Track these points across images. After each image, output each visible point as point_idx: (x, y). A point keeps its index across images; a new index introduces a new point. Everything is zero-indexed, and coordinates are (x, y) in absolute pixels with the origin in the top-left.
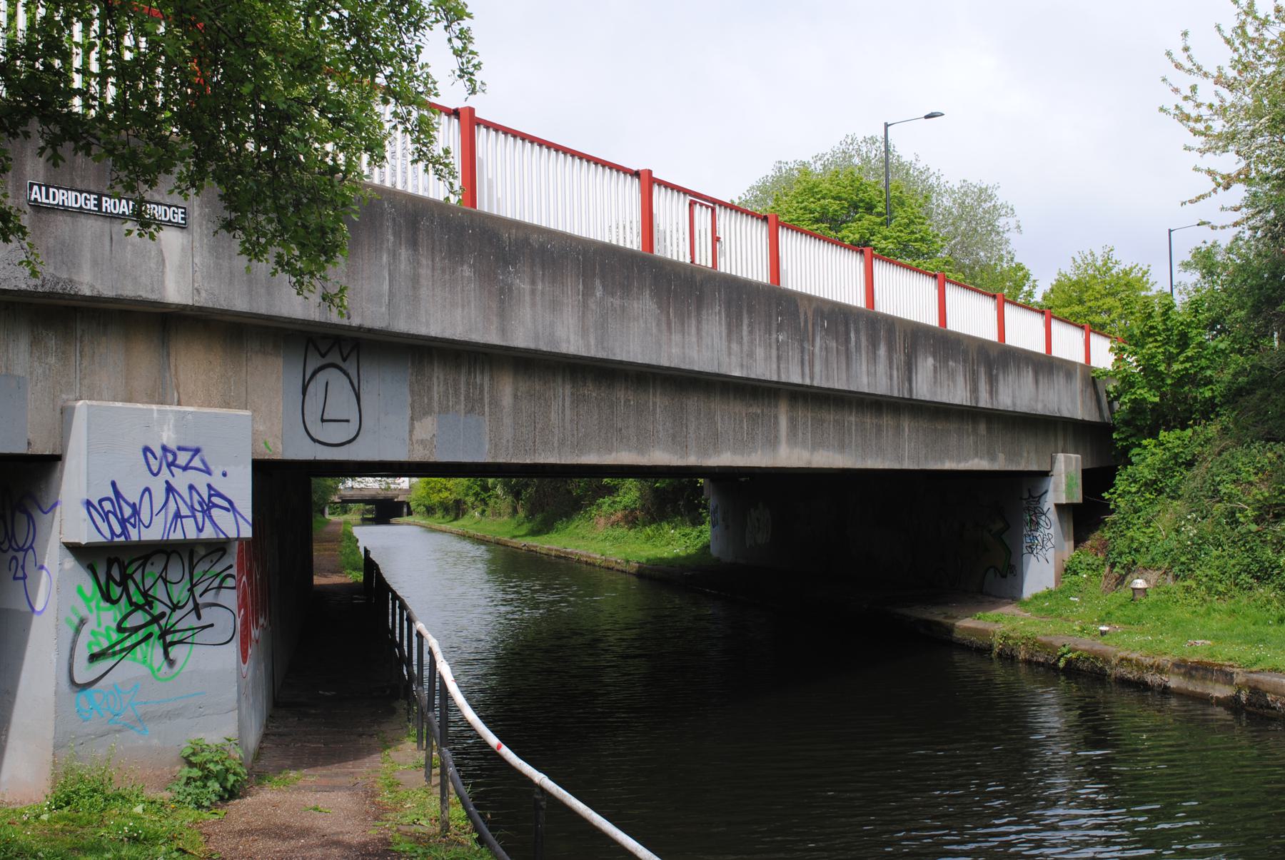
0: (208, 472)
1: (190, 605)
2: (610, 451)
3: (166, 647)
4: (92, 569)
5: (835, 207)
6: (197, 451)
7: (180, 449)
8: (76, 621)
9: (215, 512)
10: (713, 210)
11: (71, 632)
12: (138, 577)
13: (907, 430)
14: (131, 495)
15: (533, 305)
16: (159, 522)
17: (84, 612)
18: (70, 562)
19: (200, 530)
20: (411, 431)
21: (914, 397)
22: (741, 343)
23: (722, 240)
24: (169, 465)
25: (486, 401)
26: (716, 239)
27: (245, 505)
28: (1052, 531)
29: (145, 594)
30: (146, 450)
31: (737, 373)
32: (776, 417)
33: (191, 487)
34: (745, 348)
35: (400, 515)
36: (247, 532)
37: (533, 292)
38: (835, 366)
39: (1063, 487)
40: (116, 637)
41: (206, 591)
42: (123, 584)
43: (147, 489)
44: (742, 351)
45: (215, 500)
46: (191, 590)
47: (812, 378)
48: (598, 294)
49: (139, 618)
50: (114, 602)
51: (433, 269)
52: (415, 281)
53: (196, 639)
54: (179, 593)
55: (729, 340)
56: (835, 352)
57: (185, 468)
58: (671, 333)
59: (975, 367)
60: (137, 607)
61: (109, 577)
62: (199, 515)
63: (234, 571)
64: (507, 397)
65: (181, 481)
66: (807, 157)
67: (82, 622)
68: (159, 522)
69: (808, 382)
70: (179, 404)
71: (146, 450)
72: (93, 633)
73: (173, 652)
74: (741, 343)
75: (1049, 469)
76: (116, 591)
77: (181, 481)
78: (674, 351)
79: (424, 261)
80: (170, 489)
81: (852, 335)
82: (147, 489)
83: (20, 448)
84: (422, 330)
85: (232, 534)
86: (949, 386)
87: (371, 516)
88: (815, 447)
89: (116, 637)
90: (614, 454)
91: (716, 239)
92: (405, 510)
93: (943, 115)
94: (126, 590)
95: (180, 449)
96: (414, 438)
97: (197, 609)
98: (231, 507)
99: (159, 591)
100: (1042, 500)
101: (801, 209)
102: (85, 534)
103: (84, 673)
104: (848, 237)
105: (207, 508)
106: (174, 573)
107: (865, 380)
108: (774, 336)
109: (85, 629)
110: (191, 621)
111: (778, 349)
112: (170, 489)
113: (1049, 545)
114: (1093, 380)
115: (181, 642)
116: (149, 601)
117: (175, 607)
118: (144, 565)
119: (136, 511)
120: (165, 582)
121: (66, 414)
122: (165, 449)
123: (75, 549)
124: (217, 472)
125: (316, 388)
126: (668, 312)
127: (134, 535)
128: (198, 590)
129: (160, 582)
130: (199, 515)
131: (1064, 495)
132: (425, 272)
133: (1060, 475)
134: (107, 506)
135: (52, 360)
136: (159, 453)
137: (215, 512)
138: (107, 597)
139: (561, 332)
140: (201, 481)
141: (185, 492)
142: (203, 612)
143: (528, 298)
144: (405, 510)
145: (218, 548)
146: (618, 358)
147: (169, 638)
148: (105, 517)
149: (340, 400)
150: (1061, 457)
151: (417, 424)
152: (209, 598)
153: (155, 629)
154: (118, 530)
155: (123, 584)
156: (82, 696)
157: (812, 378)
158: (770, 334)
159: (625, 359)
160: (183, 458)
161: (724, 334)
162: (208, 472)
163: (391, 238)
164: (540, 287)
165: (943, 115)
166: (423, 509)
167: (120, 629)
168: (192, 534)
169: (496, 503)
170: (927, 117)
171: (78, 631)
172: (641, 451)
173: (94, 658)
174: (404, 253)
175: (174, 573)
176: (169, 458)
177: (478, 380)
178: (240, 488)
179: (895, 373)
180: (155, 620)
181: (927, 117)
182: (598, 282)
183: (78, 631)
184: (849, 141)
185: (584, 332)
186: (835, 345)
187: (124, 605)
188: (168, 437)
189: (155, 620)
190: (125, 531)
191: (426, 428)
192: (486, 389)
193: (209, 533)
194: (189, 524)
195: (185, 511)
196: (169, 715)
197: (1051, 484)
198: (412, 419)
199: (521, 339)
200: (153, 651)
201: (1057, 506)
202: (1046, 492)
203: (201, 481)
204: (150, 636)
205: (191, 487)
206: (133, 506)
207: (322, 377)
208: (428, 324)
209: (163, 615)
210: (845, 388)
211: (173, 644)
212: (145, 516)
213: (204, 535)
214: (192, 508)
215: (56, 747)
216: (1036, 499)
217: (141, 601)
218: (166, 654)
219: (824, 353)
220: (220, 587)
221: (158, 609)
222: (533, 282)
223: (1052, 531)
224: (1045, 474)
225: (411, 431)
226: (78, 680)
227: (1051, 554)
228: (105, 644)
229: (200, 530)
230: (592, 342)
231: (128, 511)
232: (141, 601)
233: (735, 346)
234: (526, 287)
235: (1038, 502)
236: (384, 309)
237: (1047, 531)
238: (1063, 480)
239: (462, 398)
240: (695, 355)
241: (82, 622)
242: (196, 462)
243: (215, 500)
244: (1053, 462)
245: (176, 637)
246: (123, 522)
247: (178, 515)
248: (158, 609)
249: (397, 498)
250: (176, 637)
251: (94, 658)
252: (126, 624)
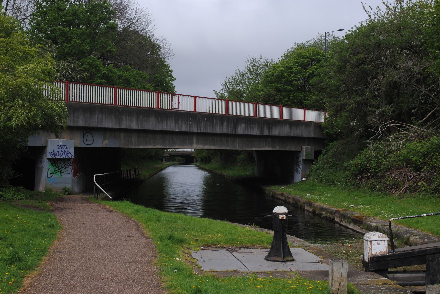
0: (67, 149)
1: (65, 167)
2: (146, 146)
3: (61, 173)
4: (50, 162)
5: (306, 61)
6: (65, 146)
7: (63, 145)
8: (48, 168)
9: (68, 154)
10: (178, 96)
11: (48, 170)
12: (57, 163)
13: (238, 141)
14: (56, 152)
15: (126, 121)
16: (60, 155)
17: (49, 167)
18: (47, 161)
19: (66, 157)
20: (103, 142)
21: (237, 133)
22: (179, 124)
23: (180, 102)
24: (61, 148)
25: (118, 137)
26: (179, 102)
27: (73, 154)
28: (301, 166)
29: (58, 166)
30: (58, 146)
31: (177, 130)
32: (192, 139)
33: (64, 151)
34: (180, 125)
35: (193, 162)
36: (73, 157)
37: (126, 119)
38: (208, 128)
39: (304, 155)
40: (54, 171)
41: (67, 166)
42: (55, 164)
43: (58, 151)
44: (179, 126)
45: (68, 153)
46: (65, 165)
47: (200, 130)
48: (141, 118)
49: (57, 169)
50: (54, 166)
51: (106, 117)
52: (102, 119)
53: (65, 172)
54: (63, 166)
55: (175, 124)
56: (208, 125)
57: (64, 148)
58: (159, 124)
59: (262, 126)
60: (57, 167)
61: (53, 163)
62: (66, 155)
63: (72, 163)
64: (122, 137)
65: (63, 150)
66: (304, 42)
67: (49, 169)
68: (60, 155)
69: (199, 131)
70: (63, 139)
71: (58, 146)
72: (51, 170)
73: (62, 174)
74: (179, 124)
75: (301, 150)
76: (54, 165)
77: (63, 150)
78: (160, 127)
79: (104, 115)
80: (61, 151)
81: (215, 121)
82: (58, 151)
83: (41, 145)
84: (103, 127)
85: (71, 158)
86: (251, 130)
87: (183, 162)
88: (204, 145)
89: (54, 171)
90: (147, 146)
91: (179, 102)
92: (195, 160)
93: (344, 30)
94: (55, 165)
95: (63, 145)
96: (103, 143)
97: (66, 168)
98: (71, 154)
99: (60, 165)
100: (299, 158)
101: (295, 62)
102: (49, 157)
103: (49, 176)
104: (309, 72)
105: (67, 154)
106: (62, 163)
107: (219, 130)
108: (189, 122)
109: (49, 170)
110: (65, 170)
111: (190, 125)
112: (61, 151)
113: (301, 170)
114: (317, 125)
115: (63, 173)
116: (58, 167)
117: (62, 168)
118: (58, 162)
119: (56, 154)
120: (61, 164)
121: (47, 141)
122: (61, 145)
123: (48, 159)
124: (68, 149)
125: (85, 136)
126: (159, 120)
127: (56, 157)
128: (66, 165)
129: (60, 164)
130: (66, 155)
131: (304, 157)
132: (104, 117)
133: (304, 152)
134: (52, 153)
135: (45, 133)
136: (60, 146)
137: (68, 154)
138: (52, 166)
139: (132, 125)
140: (66, 150)
141: (64, 152)
142: (66, 169)
143: (125, 120)
144: (195, 160)
145: (69, 159)
146: (146, 129)
147: (61, 172)
148: (52, 155)
149: (90, 138)
150: (304, 147)
151: (104, 141)
152: (67, 167)
153: (59, 170)
154: (54, 156)
155: (55, 164)
156: (49, 179)
157: (200, 130)
158: (187, 122)
159: (147, 129)
160: (63, 147)
161: (174, 123)
162: (67, 149)
163: (98, 112)
164: (128, 118)
165: (344, 30)
166: (200, 160)
167: (54, 170)
168: (64, 157)
169: (217, 157)
170: (339, 30)
171: (48, 170)
172: (154, 146)
173: (51, 174)
174: (100, 115)
175: (62, 163)
176: (61, 146)
177: (116, 134)
178: (72, 151)
179: (230, 128)
180: (59, 169)
181: (339, 30)
182: (141, 116)
183: (48, 170)
184: (320, 35)
185: (138, 125)
186: (208, 123)
187: (55, 167)
188: (61, 144)
189: (59, 169)
190: (55, 157)
191: (106, 142)
192: (118, 135)
193: (67, 157)
194: (64, 156)
195: (63, 154)
196: (61, 183)
197: (301, 154)
198: (103, 140)
199: (123, 126)
200: (59, 173)
201: (303, 160)
202: (300, 156)
203: (66, 150)
204: (59, 171)
205: (64, 151)
206: (56, 153)
207: (86, 134)
208: (104, 126)
209: (60, 169)
210: (212, 132)
211: (62, 173)
212: (58, 155)
213: (66, 158)
214: (65, 154)
215: (45, 185)
216: (298, 158)
217: (57, 166)
218: (61, 174)
219: (205, 125)
220: (69, 165)
221: (60, 168)
222: (126, 117)
223: (301, 166)
224: (300, 152)
225: (103, 142)
226: (48, 176)
227: (301, 172)
228: (52, 172)
229: (66, 157)
230: (139, 126)
231: (55, 154)
232: (57, 166)
233: (177, 125)
234: (125, 118)
235: (298, 159)
236: (96, 124)
237: (300, 166)
238: (304, 153)
239: (113, 137)
240: (166, 128)
241: (49, 169)
242: (65, 147)
243: (68, 153)
244: (302, 148)
245: (62, 172)
246: (55, 155)
247: (62, 155)
248: (60, 168)
249: (192, 155)
250: (62, 172)
251: (51, 174)
252: (55, 169)
